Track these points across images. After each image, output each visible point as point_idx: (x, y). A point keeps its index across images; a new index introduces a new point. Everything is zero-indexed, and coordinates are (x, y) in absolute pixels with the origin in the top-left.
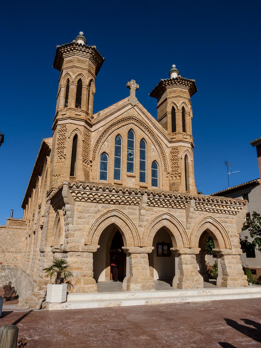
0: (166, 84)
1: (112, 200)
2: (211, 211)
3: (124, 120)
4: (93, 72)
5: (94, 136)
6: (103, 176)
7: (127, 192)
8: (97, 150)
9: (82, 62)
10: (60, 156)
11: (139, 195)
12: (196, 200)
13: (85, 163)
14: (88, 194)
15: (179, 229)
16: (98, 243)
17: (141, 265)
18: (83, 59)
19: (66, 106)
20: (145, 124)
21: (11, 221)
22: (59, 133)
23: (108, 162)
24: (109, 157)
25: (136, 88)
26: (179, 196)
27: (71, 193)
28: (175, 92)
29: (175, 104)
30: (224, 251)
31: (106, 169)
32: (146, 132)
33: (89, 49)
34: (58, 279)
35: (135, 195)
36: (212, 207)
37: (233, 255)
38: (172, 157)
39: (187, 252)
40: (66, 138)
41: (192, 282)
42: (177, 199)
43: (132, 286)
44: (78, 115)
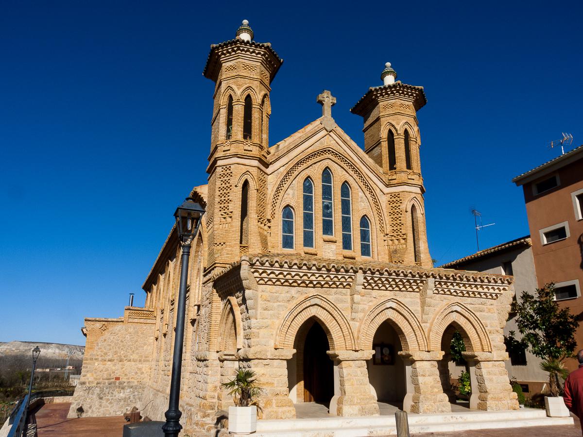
0: (378, 95)
1: (311, 282)
2: (459, 295)
3: (315, 154)
4: (267, 82)
5: (272, 181)
6: (288, 242)
7: (333, 269)
8: (276, 202)
9: (249, 68)
10: (223, 214)
11: (351, 273)
12: (435, 278)
13: (261, 223)
14: (277, 274)
15: (411, 322)
16: (294, 346)
17: (357, 377)
19: (228, 137)
20: (348, 159)
21: (132, 311)
22: (220, 179)
23: (294, 220)
24: (295, 213)
25: (331, 103)
26: (410, 273)
27: (253, 273)
28: (392, 106)
29: (393, 126)
30: (480, 355)
31: (291, 231)
33: (261, 48)
34: (243, 399)
35: (344, 273)
36: (460, 287)
37: (495, 361)
38: (392, 209)
40: (231, 186)
41: (434, 403)
42: (407, 278)
43: (346, 409)
44: (249, 151)
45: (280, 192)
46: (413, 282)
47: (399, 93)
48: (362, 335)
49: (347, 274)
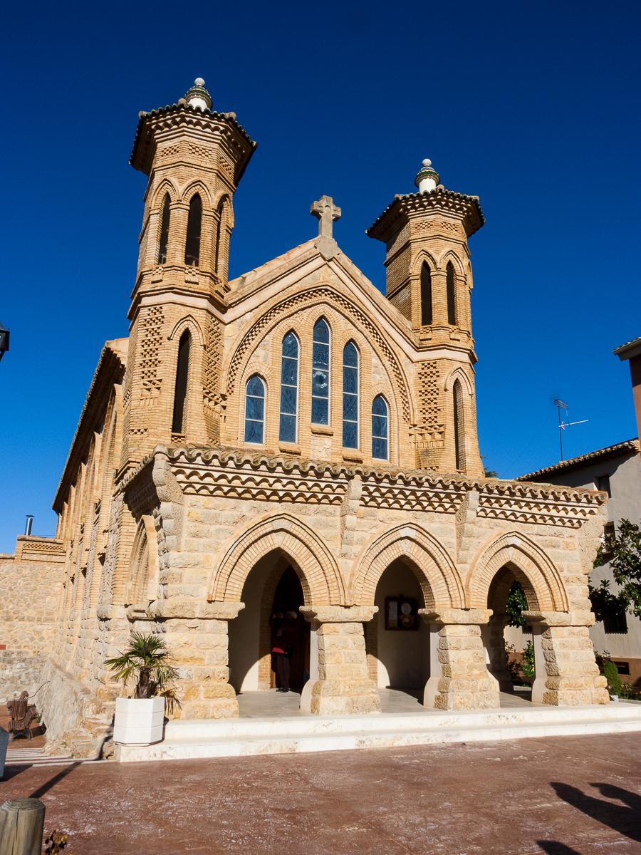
0: (409, 207)
1: (275, 492)
2: (519, 519)
3: (304, 295)
4: (230, 177)
5: (231, 335)
6: (254, 433)
7: (312, 472)
8: (237, 369)
9: (200, 152)
10: (147, 383)
12: (480, 491)
13: (210, 400)
14: (216, 477)
15: (439, 562)
17: (346, 651)
19: (161, 260)
21: (28, 543)
22: (145, 328)
25: (333, 215)
26: (440, 481)
27: (175, 474)
28: (429, 225)
29: (430, 256)
30: (549, 616)
31: (260, 416)
33: (219, 120)
36: (521, 507)
37: (573, 626)
38: (424, 386)
40: (161, 338)
41: (472, 692)
42: (435, 490)
43: (324, 702)
45: (244, 353)
46: (445, 497)
47: (441, 204)
48: (358, 580)
49: (335, 481)
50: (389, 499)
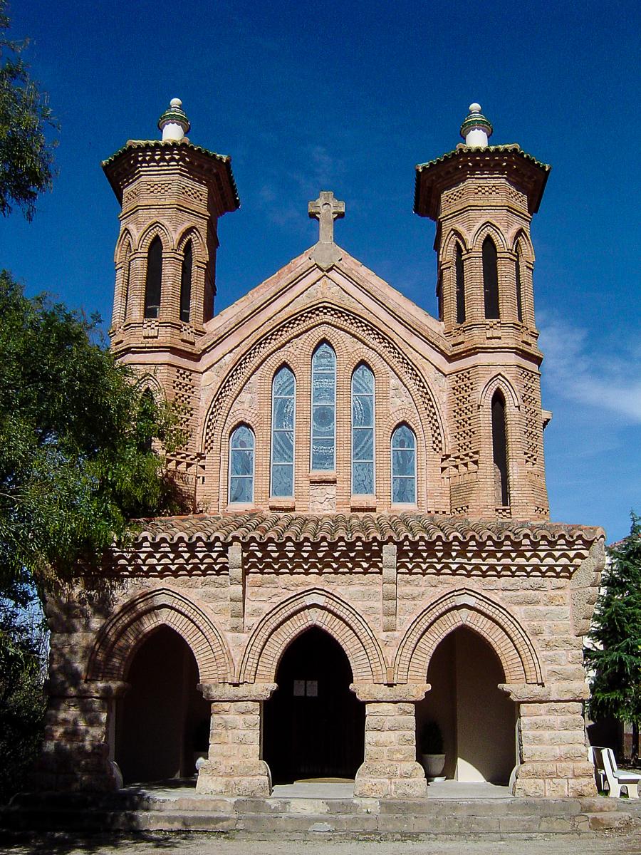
3: (296, 319)
5: (207, 383)
18: (164, 179)
25: (334, 213)
32: (369, 340)
39: (379, 697)
50: (183, 554)
